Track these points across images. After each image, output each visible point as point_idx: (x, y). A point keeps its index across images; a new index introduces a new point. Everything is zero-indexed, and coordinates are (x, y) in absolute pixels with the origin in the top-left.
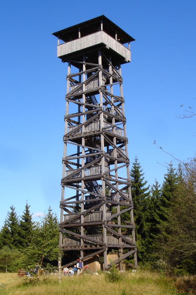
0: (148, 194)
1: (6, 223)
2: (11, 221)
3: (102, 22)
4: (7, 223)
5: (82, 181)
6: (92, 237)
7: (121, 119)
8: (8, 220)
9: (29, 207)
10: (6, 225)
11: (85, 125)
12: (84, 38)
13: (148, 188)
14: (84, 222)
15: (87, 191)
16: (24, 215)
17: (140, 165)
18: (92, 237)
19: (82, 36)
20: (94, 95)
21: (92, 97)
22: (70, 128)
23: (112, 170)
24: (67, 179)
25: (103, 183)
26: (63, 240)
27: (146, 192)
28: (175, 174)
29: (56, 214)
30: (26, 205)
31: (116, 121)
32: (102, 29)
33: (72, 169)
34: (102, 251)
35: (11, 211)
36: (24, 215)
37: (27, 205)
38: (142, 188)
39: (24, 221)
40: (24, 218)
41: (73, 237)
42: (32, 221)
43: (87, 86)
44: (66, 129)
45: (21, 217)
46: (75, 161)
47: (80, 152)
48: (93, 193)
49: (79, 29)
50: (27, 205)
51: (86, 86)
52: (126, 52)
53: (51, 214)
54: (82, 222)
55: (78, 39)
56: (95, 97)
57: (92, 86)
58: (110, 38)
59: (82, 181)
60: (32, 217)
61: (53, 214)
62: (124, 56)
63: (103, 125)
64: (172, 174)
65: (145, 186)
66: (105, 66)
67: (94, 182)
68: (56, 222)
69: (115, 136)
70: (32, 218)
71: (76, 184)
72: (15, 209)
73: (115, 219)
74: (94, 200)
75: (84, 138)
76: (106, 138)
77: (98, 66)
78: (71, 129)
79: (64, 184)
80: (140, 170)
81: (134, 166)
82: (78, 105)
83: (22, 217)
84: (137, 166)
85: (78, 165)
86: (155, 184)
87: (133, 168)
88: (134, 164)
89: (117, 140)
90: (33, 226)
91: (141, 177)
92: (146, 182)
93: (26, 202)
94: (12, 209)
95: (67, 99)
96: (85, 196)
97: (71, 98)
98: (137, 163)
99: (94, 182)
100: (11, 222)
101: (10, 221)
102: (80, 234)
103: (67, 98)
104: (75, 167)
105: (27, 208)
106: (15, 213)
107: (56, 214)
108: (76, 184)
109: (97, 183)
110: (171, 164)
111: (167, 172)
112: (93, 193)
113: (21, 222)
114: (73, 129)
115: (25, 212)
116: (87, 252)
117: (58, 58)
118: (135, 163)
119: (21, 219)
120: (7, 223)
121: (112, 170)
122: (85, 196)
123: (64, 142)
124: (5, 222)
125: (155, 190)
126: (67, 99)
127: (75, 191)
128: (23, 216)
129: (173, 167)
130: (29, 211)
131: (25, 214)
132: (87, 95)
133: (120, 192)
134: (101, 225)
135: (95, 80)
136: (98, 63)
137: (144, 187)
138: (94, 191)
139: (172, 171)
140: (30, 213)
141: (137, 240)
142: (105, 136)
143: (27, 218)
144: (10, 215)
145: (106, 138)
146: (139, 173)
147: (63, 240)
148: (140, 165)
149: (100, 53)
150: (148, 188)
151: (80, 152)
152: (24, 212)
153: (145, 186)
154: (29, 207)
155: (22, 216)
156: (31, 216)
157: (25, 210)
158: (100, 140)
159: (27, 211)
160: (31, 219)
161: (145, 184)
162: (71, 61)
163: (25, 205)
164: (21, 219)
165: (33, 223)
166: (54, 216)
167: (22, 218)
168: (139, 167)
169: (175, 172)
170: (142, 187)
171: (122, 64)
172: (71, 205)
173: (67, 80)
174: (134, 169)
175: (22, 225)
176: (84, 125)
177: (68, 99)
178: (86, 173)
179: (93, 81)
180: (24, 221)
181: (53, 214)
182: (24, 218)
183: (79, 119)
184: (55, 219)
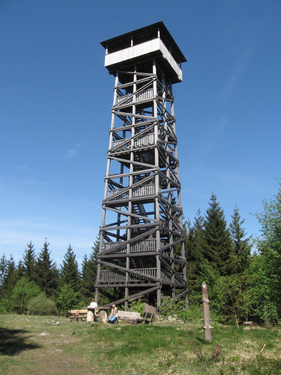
3: (154, 63)
6: (141, 271)
7: (176, 186)
11: (136, 95)
14: (130, 253)
18: (141, 271)
19: (134, 44)
22: (110, 192)
24: (109, 201)
26: (101, 275)
31: (172, 186)
34: (154, 289)
35: (28, 249)
36: (42, 253)
37: (46, 243)
41: (115, 271)
43: (137, 98)
44: (106, 193)
51: (136, 98)
52: (178, 70)
54: (128, 252)
57: (142, 193)
63: (157, 189)
73: (168, 250)
75: (133, 164)
78: (111, 194)
79: (105, 206)
94: (30, 246)
95: (104, 205)
102: (125, 267)
103: (104, 204)
105: (46, 246)
114: (115, 193)
116: (133, 291)
126: (104, 205)
128: (41, 253)
130: (48, 250)
131: (43, 252)
132: (134, 203)
135: (147, 91)
140: (49, 252)
141: (198, 341)
143: (45, 255)
147: (101, 275)
149: (154, 63)
155: (40, 253)
159: (46, 249)
162: (119, 72)
173: (110, 135)
175: (40, 263)
176: (133, 139)
177: (115, 111)
179: (144, 187)
180: (42, 259)
182: (41, 256)
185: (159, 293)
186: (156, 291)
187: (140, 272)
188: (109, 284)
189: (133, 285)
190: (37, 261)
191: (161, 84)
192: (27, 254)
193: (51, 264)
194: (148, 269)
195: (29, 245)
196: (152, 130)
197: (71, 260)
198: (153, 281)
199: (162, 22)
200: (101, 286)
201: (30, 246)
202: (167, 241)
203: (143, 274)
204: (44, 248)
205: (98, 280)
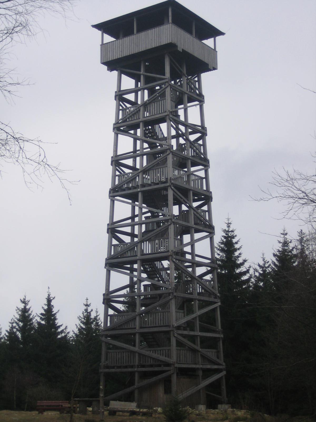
0: (248, 280)
1: (12, 326)
2: (22, 323)
4: (14, 325)
5: (139, 262)
8: (17, 321)
9: (52, 299)
10: (12, 328)
12: (143, 34)
13: (248, 271)
15: (146, 276)
16: (44, 312)
17: (235, 233)
19: (139, 31)
20: (160, 261)
21: (157, 126)
23: (187, 244)
25: (180, 109)
27: (245, 278)
28: (291, 248)
29: (97, 312)
30: (47, 296)
32: (170, 21)
33: (123, 242)
34: (168, 373)
35: (22, 306)
36: (44, 312)
37: (49, 295)
38: (238, 271)
39: (43, 322)
40: (43, 317)
42: (59, 322)
45: (39, 316)
46: (128, 229)
47: (136, 214)
48: (155, 281)
49: (135, 19)
50: (49, 295)
53: (89, 311)
55: (133, 36)
56: (159, 127)
58: (187, 36)
59: (139, 262)
60: (58, 316)
61: (92, 310)
62: (206, 61)
64: (286, 248)
65: (243, 269)
66: (175, 75)
67: (157, 264)
68: (97, 324)
69: (190, 190)
70: (57, 317)
71: (129, 266)
72: (29, 303)
74: (158, 292)
76: (177, 194)
77: (165, 79)
80: (234, 241)
81: (225, 235)
82: (133, 139)
83: (41, 316)
84: (230, 235)
85: (132, 235)
86: (262, 263)
87: (223, 238)
88: (225, 231)
89: (195, 195)
90: (59, 330)
91: (237, 254)
92: (245, 261)
93: (47, 290)
94: (24, 302)
96: (143, 285)
97: (122, 128)
98: (230, 230)
99: (157, 264)
100: (21, 324)
101: (20, 323)
102: (134, 346)
104: (127, 239)
105: (49, 301)
106: (29, 309)
107: (97, 312)
108: (129, 266)
109: (162, 264)
110: (285, 232)
111: (279, 247)
112: (155, 281)
113: (39, 323)
115: (46, 307)
117: (94, 29)
118: (227, 229)
119: (39, 320)
120: (14, 325)
121: (187, 244)
122: (143, 285)
123: (109, 198)
124: (10, 323)
125: (261, 272)
127: (128, 277)
128: (42, 314)
129: (288, 237)
130: (53, 306)
131: (45, 310)
133: (199, 279)
134: (168, 332)
136: (164, 74)
137: (241, 269)
138: (158, 278)
139: (285, 244)
140: (55, 310)
142: (174, 189)
144: (20, 313)
145: (175, 192)
146: (234, 246)
148: (235, 233)
150: (248, 271)
151: (136, 214)
152: (43, 308)
153: (243, 269)
154: (52, 299)
156: (55, 314)
157: (45, 304)
158: (167, 196)
160: (55, 319)
161: (242, 264)
163: (46, 296)
164: (39, 320)
165: (59, 327)
166: (93, 315)
167: (41, 318)
168: (233, 237)
169: (291, 246)
170: (237, 268)
171: (185, 247)
172: (122, 299)
174: (225, 240)
178: (147, 248)
181: (92, 310)
183: (135, 161)
184: (95, 318)
185: (174, 379)
186: (170, 376)
187: (153, 352)
188: (116, 368)
189: (144, 369)
190: (36, 325)
191: (180, 68)
192: (19, 315)
193: (59, 330)
194: (164, 348)
195: (22, 299)
196: (112, 192)
197: (211, 278)
198: (168, 365)
199: (108, 70)
200: (107, 370)
201: (24, 302)
202: (190, 311)
203: (155, 355)
204: (46, 303)
205: (103, 362)
